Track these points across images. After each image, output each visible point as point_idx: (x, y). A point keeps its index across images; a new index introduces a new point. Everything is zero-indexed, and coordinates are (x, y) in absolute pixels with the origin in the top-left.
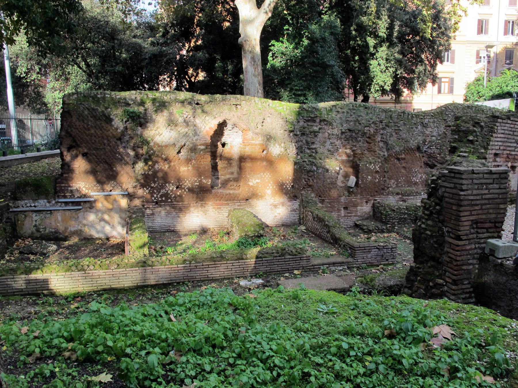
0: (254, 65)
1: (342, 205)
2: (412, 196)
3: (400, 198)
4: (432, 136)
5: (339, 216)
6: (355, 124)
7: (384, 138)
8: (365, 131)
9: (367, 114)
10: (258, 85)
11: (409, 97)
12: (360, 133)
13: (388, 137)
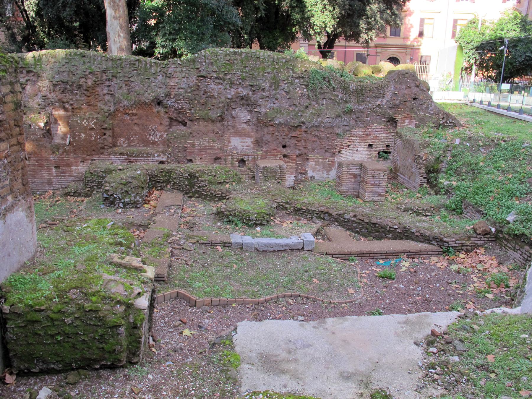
0: (113, 6)
1: (51, 164)
2: (141, 157)
3: (126, 159)
4: (179, 88)
5: (50, 175)
6: (68, 75)
7: (111, 91)
8: (81, 83)
9: (84, 63)
10: (119, 28)
11: (417, 42)
12: (75, 85)
13: (116, 89)
